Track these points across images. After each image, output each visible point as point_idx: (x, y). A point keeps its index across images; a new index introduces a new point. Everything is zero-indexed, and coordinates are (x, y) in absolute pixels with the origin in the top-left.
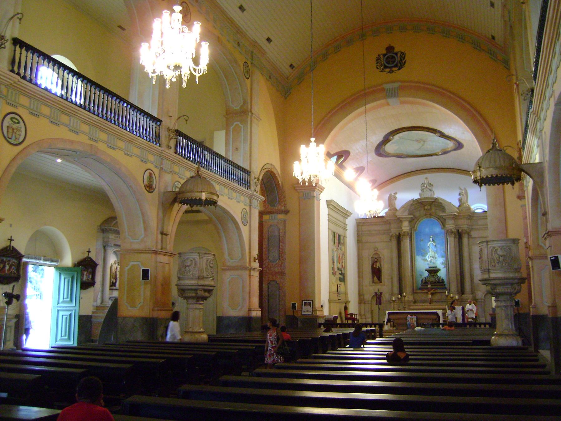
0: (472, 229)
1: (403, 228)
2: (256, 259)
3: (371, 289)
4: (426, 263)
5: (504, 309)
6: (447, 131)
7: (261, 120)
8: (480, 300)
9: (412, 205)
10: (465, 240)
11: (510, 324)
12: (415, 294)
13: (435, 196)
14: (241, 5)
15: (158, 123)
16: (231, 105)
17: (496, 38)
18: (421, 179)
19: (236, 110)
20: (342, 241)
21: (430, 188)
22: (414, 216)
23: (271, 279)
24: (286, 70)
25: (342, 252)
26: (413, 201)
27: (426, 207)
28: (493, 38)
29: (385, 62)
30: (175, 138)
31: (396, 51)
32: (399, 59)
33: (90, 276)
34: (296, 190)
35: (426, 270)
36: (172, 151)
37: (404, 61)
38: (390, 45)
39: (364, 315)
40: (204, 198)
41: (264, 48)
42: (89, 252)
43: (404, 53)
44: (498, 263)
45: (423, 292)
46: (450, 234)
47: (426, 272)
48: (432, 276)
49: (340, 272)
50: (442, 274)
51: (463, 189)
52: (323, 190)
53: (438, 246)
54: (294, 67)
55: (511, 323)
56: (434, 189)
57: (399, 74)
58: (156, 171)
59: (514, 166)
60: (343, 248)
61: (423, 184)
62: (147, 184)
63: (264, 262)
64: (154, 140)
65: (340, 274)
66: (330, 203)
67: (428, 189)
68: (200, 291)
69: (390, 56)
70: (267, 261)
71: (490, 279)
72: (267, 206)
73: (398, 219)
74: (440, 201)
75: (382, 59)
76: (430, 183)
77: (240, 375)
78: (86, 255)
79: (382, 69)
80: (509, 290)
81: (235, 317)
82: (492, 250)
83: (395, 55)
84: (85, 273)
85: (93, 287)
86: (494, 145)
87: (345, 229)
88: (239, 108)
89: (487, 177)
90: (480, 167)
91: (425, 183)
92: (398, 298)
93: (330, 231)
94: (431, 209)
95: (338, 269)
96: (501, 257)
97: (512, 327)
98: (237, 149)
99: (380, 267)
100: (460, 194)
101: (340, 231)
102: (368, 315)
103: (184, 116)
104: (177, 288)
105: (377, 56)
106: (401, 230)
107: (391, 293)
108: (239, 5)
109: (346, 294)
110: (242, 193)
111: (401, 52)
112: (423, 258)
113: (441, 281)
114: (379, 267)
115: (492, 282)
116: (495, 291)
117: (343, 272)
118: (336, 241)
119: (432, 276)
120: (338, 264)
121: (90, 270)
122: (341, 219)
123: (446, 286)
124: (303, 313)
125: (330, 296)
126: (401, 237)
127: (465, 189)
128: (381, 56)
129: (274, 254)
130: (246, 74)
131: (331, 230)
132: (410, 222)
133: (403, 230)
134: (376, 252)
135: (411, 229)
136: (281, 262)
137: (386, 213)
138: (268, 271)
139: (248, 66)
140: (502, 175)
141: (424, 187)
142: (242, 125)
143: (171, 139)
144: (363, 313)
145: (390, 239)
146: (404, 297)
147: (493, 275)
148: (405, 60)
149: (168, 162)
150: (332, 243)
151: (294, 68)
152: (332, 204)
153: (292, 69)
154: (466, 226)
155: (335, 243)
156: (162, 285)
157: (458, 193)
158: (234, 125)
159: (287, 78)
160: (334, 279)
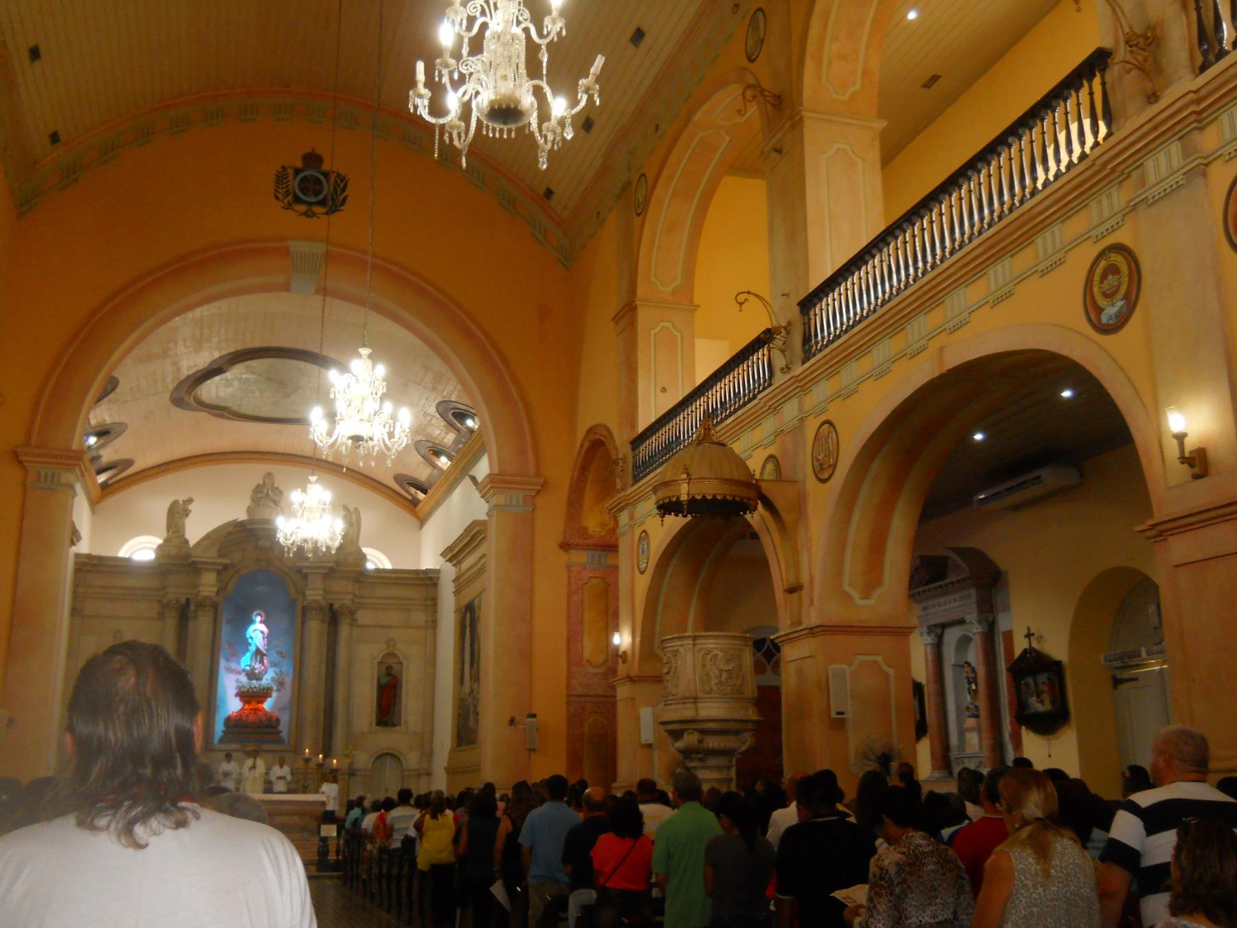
1: (308, 592)
7: (699, 306)
10: (344, 630)
17: (555, 198)
28: (549, 193)
29: (296, 186)
31: (326, 167)
32: (332, 189)
38: (313, 150)
43: (344, 178)
51: (352, 510)
68: (689, 734)
69: (312, 176)
71: (699, 718)
82: (703, 656)
83: (322, 178)
96: (724, 673)
105: (280, 169)
111: (338, 175)
126: (192, 608)
128: (290, 171)
132: (219, 573)
136: (832, 667)
140: (714, 496)
141: (262, 495)
154: (351, 597)
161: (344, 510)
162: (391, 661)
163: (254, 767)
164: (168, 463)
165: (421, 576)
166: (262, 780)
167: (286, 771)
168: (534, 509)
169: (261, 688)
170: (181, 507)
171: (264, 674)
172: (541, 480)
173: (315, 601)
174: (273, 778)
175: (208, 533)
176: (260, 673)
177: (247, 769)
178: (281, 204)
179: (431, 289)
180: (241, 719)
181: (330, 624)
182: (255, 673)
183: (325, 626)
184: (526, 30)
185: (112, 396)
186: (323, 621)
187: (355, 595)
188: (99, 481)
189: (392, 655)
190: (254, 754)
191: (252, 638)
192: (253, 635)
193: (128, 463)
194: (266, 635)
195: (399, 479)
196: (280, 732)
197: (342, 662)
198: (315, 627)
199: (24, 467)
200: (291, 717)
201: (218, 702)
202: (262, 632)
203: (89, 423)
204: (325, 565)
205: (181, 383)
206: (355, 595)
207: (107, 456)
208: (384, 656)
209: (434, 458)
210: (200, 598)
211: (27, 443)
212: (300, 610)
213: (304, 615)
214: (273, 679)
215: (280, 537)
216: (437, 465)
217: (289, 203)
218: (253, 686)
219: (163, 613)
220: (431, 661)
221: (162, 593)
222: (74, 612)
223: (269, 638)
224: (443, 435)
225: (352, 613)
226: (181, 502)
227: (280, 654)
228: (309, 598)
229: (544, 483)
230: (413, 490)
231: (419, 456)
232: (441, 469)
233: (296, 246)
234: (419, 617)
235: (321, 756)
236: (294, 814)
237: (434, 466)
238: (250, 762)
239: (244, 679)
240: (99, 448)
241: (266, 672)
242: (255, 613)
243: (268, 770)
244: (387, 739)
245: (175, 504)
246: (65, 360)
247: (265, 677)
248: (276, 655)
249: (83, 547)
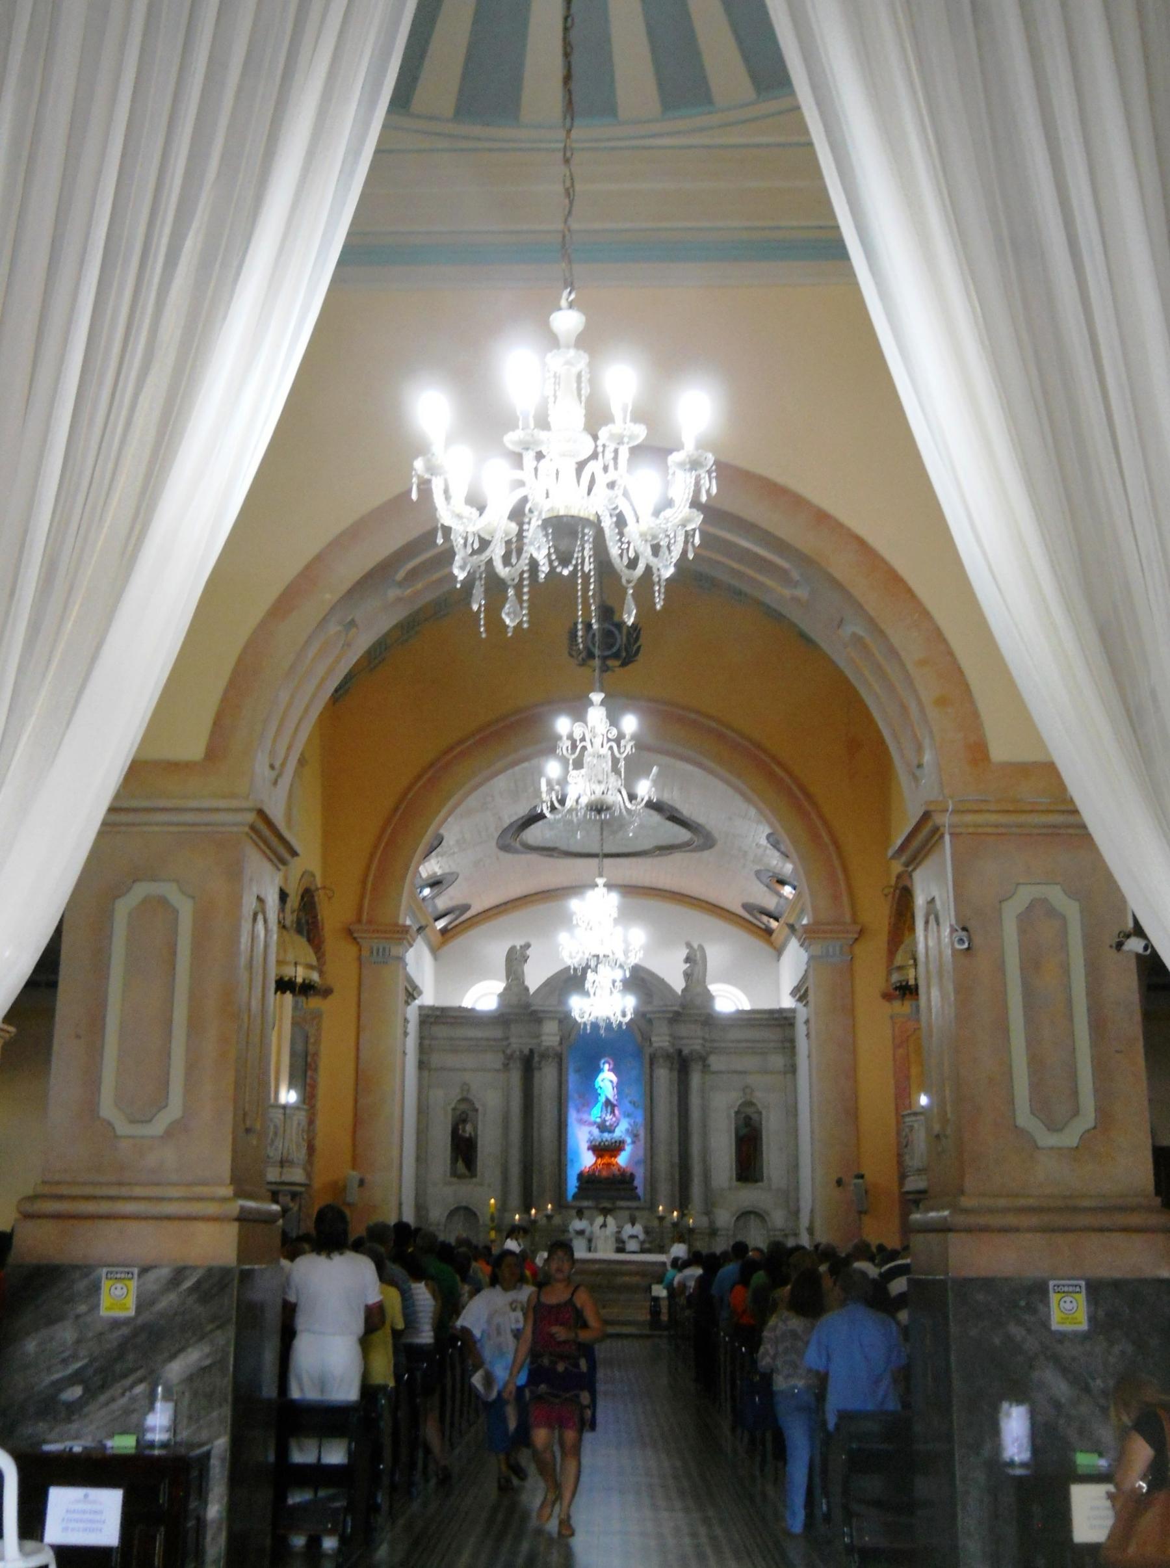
1: (653, 1039)
8: (723, 1233)
10: (696, 1079)
37: (636, 646)
40: (299, 980)
73: (534, 1013)
99: (473, 1133)
114: (470, 1134)
126: (536, 1059)
127: (701, 948)
148: (638, 644)
154: (700, 1041)
161: (688, 948)
162: (749, 1111)
163: (604, 1225)
164: (506, 903)
165: (776, 1016)
166: (613, 1239)
167: (638, 1229)
168: (852, 958)
169: (613, 1141)
170: (518, 953)
171: (616, 1127)
172: (858, 928)
173: (661, 1048)
174: (625, 1236)
175: (548, 979)
176: (611, 1125)
177: (598, 1228)
179: (728, 732)
180: (594, 1174)
181: (680, 1071)
182: (606, 1126)
183: (675, 1074)
184: (611, 748)
185: (439, 849)
186: (671, 1069)
187: (704, 1039)
188: (438, 928)
189: (750, 1104)
190: (605, 1212)
191: (601, 1088)
192: (601, 1084)
193: (467, 908)
194: (615, 1084)
195: (746, 906)
196: (636, 1188)
197: (695, 1114)
198: (663, 1075)
199: (358, 943)
200: (646, 1170)
201: (570, 1156)
202: (611, 1081)
203: (421, 877)
204: (670, 1008)
205: (505, 831)
206: (704, 1039)
207: (442, 903)
208: (740, 1106)
209: (778, 887)
210: (543, 1048)
211: (359, 921)
212: (647, 1060)
213: (652, 1064)
214: (627, 1130)
215: (576, 1014)
216: (783, 894)
217: (583, 659)
218: (604, 1139)
219: (508, 1064)
220: (792, 1112)
221: (505, 1043)
222: (422, 1065)
223: (619, 1087)
224: (780, 865)
225: (703, 1059)
226: (518, 948)
227: (633, 1103)
228: (655, 1045)
229: (861, 931)
230: (765, 919)
231: (762, 886)
232: (787, 899)
234: (777, 1061)
235: (675, 1214)
236: (637, 1273)
237: (780, 896)
238: (600, 1220)
239: (596, 1131)
240: (433, 898)
241: (618, 1124)
242: (603, 1061)
243: (620, 1228)
244: (749, 1196)
245: (512, 950)
246: (385, 840)
247: (617, 1130)
248: (628, 1105)
249: (428, 998)
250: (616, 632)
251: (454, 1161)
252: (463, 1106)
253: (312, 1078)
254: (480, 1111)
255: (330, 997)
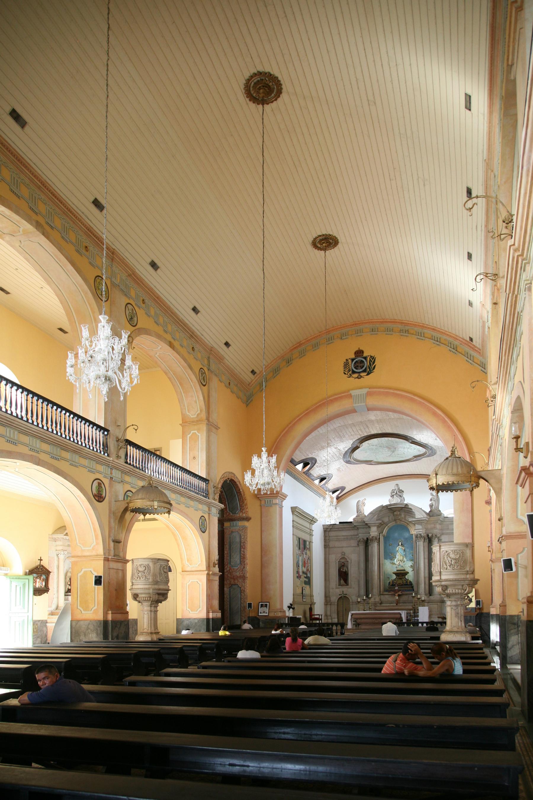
0: (443, 534)
1: (371, 533)
2: (216, 564)
3: (336, 592)
4: (395, 566)
5: (454, 608)
6: (419, 436)
9: (381, 511)
11: (460, 621)
12: (382, 596)
13: (405, 502)
14: (195, 307)
15: (106, 433)
16: (188, 413)
18: (391, 485)
19: (193, 418)
20: (308, 547)
21: (400, 494)
22: (383, 521)
23: (232, 582)
24: (248, 377)
25: (307, 557)
26: (382, 507)
27: (395, 513)
28: (471, 339)
29: (353, 366)
30: (125, 448)
33: (44, 583)
34: (258, 498)
35: (393, 573)
36: (122, 461)
39: (330, 615)
41: (222, 353)
42: (41, 560)
44: (450, 566)
45: (390, 593)
46: (419, 539)
47: (394, 575)
48: (400, 578)
49: (305, 576)
50: (410, 577)
52: (286, 497)
53: (407, 550)
54: (255, 373)
55: (461, 621)
56: (405, 495)
57: (367, 380)
58: (106, 482)
59: (471, 473)
60: (308, 552)
61: (393, 491)
62: (96, 493)
63: (226, 567)
64: (102, 450)
65: (305, 577)
66: (294, 510)
67: (399, 495)
69: (359, 360)
70: (229, 565)
72: (228, 514)
73: (367, 524)
74: (410, 507)
75: (350, 364)
76: (400, 489)
77: (187, 668)
78: (38, 563)
79: (350, 374)
80: (460, 591)
81: (195, 619)
84: (38, 580)
85: (47, 593)
86: (453, 452)
87: (311, 535)
88: (196, 416)
89: (443, 484)
90: (436, 474)
91: (395, 490)
92: (364, 600)
93: (295, 537)
94: (400, 515)
95: (303, 572)
97: (461, 624)
98: (194, 458)
100: (431, 500)
101: (306, 537)
102: (335, 616)
103: (133, 425)
104: (131, 593)
105: (345, 361)
106: (369, 535)
107: (357, 595)
108: (192, 307)
109: (311, 596)
110: (200, 502)
111: (371, 357)
112: (392, 562)
113: (408, 584)
115: (443, 583)
116: (446, 591)
117: (309, 575)
118: (302, 546)
119: (400, 578)
120: (304, 568)
121: (44, 577)
122: (307, 525)
123: (414, 588)
124: (260, 614)
125: (294, 598)
126: (369, 541)
128: (350, 361)
129: (236, 559)
130: (202, 381)
131: (296, 536)
133: (371, 535)
134: (343, 556)
135: (379, 534)
137: (354, 519)
138: (229, 575)
139: (205, 373)
140: (448, 483)
142: (199, 433)
143: (120, 448)
144: (329, 613)
145: (358, 544)
146: (370, 598)
147: (443, 577)
148: (374, 365)
149: (117, 472)
150: (297, 548)
151: (256, 375)
152: (297, 510)
153: (254, 374)
155: (300, 549)
156: (116, 590)
157: (429, 499)
158: (191, 433)
159: (249, 385)
160: (298, 582)
178: (347, 376)
198: (421, 545)
233: (354, 393)
250: (365, 361)
251: (340, 580)
252: (343, 561)
253: (243, 551)
254: (349, 562)
255: (250, 521)
